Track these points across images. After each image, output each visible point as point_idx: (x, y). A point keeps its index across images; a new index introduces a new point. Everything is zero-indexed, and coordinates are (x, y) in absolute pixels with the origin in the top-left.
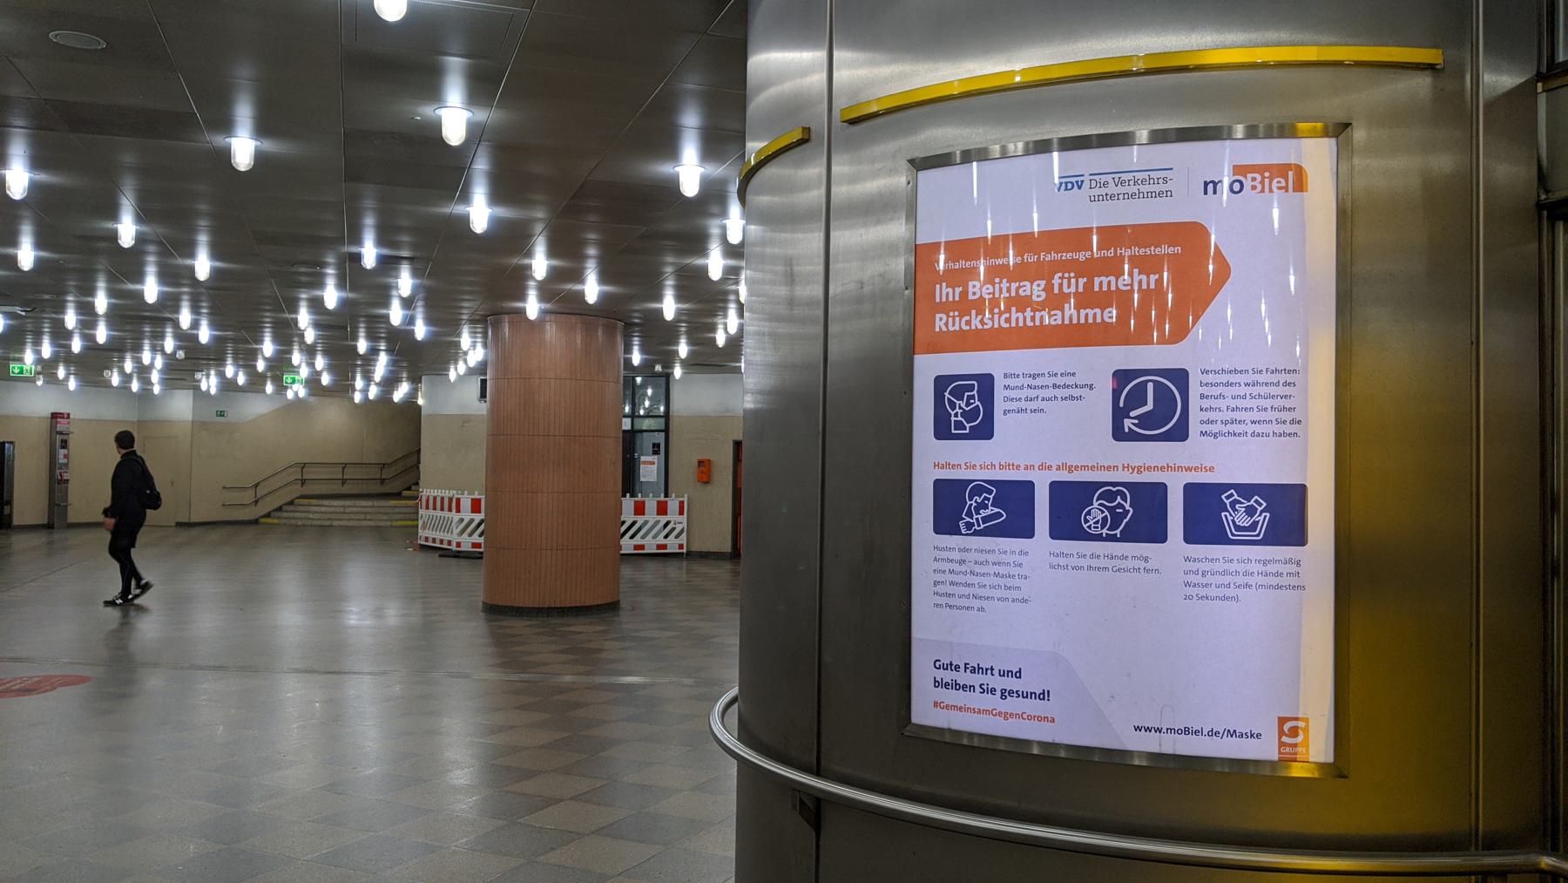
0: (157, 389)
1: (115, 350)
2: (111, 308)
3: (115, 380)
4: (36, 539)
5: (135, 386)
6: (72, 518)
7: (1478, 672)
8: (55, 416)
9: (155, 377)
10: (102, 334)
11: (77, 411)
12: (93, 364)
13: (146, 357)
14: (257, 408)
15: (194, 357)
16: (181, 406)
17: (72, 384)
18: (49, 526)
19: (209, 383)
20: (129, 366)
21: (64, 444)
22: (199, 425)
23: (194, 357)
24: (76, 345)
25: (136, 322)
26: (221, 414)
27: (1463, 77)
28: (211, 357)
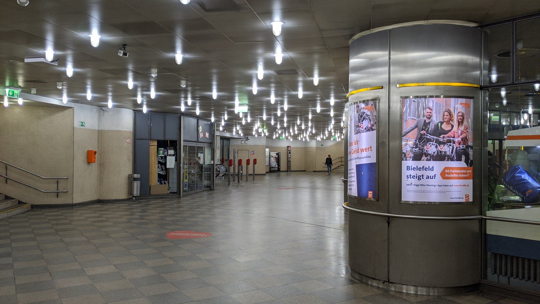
0: (308, 140)
1: (299, 134)
2: (312, 117)
3: (300, 139)
4: (285, 173)
5: (304, 140)
6: (292, 170)
7: (513, 75)
8: (288, 147)
9: (307, 138)
10: (296, 132)
11: (292, 145)
12: (295, 137)
13: (305, 135)
14: (330, 143)
15: (312, 136)
16: (313, 144)
17: (291, 140)
18: (287, 171)
19: (319, 139)
20: (302, 136)
21: (290, 153)
22: (317, 148)
23: (312, 136)
24: (292, 134)
25: (301, 131)
26: (322, 145)
27: (361, 31)
28: (317, 134)
